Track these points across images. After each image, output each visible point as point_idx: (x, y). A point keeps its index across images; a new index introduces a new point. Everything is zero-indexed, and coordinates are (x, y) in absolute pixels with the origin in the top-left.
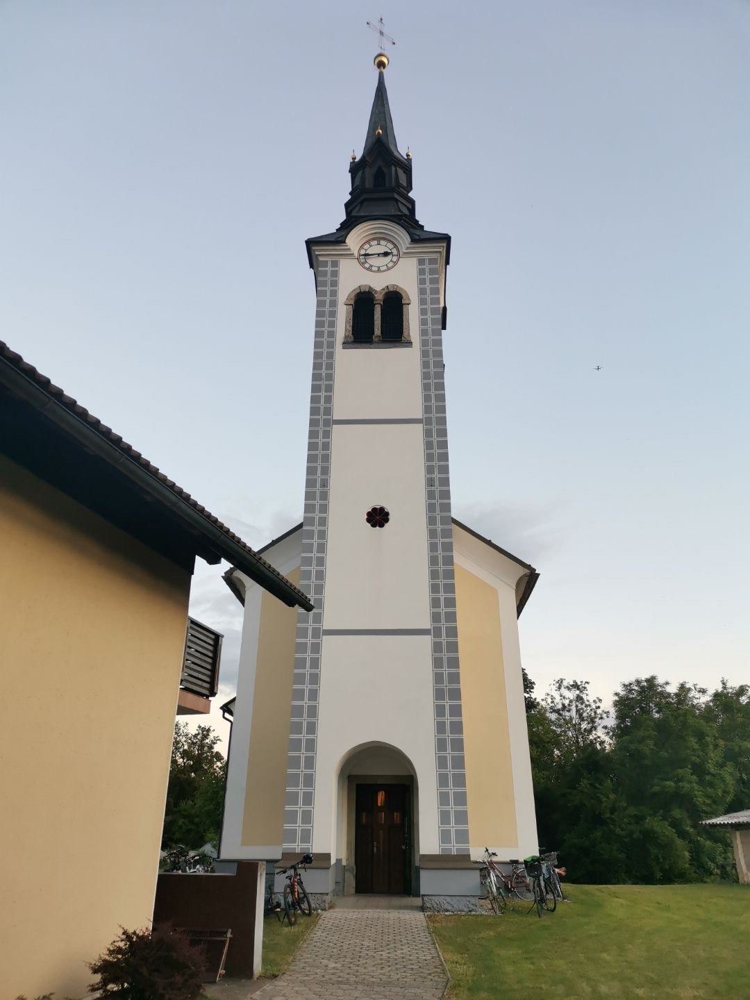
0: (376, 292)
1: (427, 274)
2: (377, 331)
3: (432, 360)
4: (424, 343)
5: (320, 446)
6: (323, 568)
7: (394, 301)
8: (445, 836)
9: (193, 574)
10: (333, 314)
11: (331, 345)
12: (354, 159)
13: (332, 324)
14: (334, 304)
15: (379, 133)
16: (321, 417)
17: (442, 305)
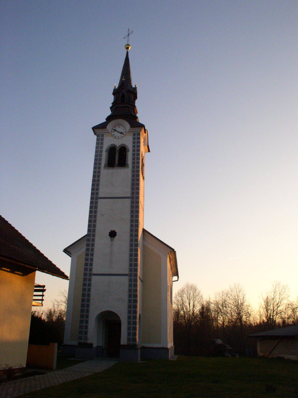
0: (117, 147)
2: (117, 163)
4: (133, 167)
5: (87, 284)
7: (123, 149)
8: (129, 339)
9: (43, 255)
10: (101, 155)
11: (100, 168)
12: (115, 87)
13: (100, 160)
14: (101, 151)
15: (123, 80)
16: (95, 196)
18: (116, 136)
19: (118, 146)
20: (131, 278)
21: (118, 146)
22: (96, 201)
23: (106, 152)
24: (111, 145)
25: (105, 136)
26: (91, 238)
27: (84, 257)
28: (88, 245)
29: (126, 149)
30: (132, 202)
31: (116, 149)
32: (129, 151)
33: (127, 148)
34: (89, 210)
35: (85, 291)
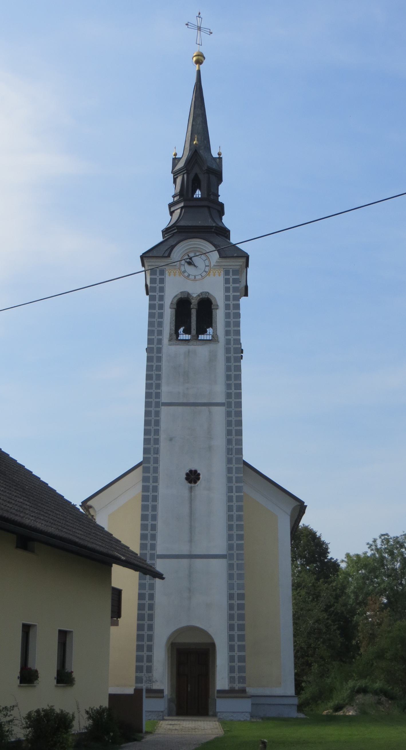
1: (233, 425)
3: (232, 346)
5: (145, 659)
6: (158, 456)
8: (232, 680)
10: (161, 316)
11: (160, 341)
13: (160, 324)
14: (161, 307)
16: (154, 400)
17: (243, 284)
18: (189, 275)
19: (195, 296)
20: (231, 562)
21: (195, 296)
22: (157, 409)
23: (170, 308)
24: (182, 293)
25: (167, 272)
26: (151, 465)
27: (139, 504)
28: (145, 479)
29: (212, 304)
30: (229, 414)
31: (190, 303)
32: (217, 307)
33: (213, 301)
34: (144, 410)
35: (144, 620)
